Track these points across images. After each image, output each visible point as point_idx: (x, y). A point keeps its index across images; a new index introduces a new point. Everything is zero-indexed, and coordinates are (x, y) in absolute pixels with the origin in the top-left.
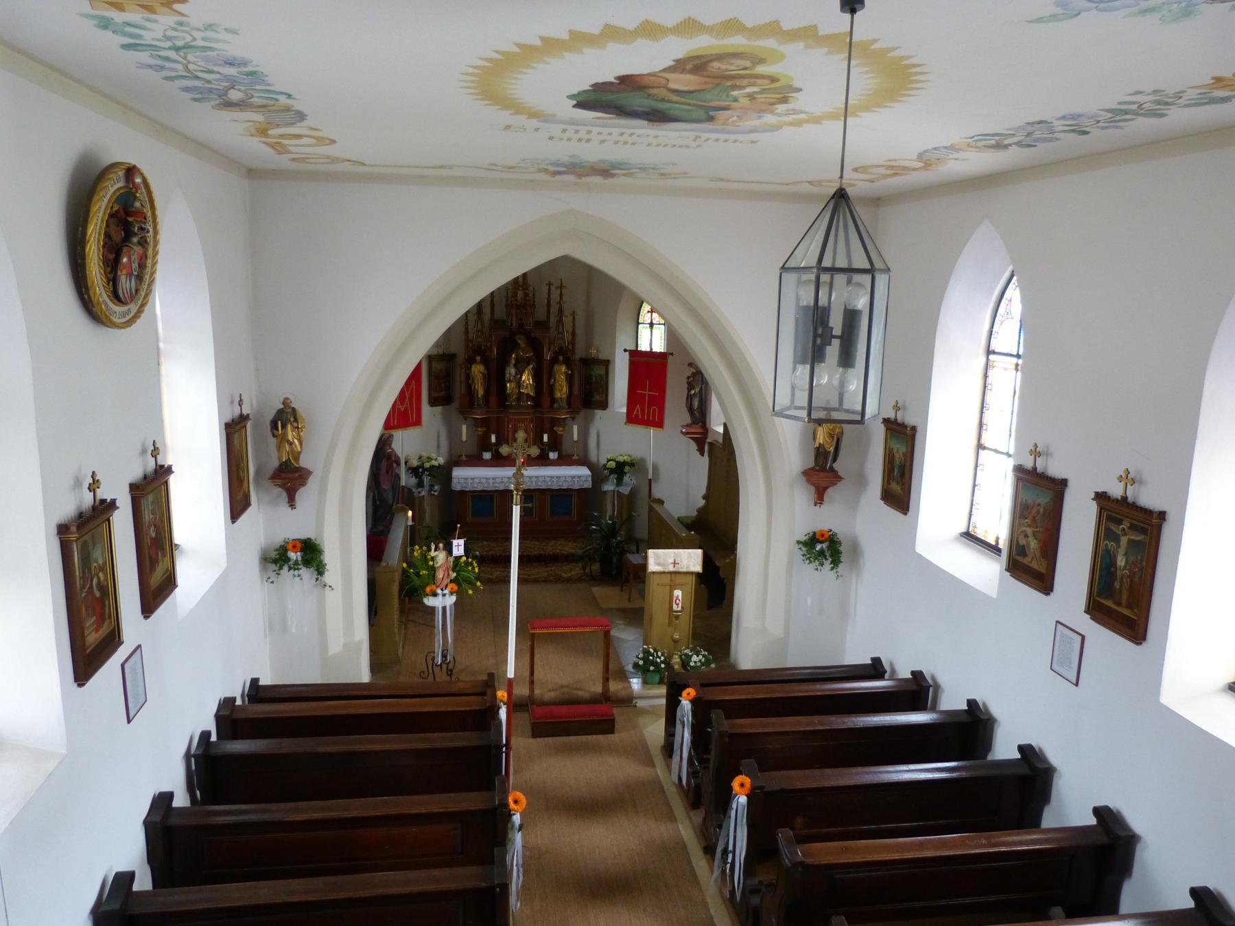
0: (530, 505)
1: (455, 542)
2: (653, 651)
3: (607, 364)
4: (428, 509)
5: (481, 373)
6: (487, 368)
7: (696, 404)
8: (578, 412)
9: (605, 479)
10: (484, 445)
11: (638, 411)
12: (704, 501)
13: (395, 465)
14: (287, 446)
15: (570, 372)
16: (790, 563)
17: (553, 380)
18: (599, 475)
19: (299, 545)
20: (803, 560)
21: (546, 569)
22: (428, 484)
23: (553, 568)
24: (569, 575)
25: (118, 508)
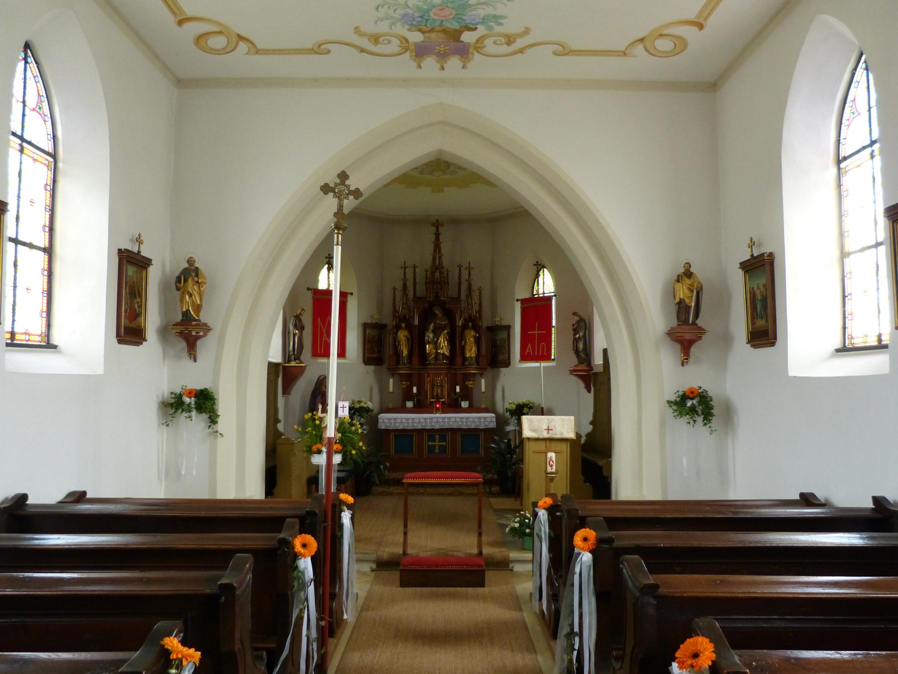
0: (444, 443)
3: (508, 328)
5: (405, 336)
7: (581, 346)
10: (408, 395)
11: (529, 349)
12: (591, 426)
14: (187, 297)
15: (478, 335)
16: (663, 424)
17: (463, 342)
20: (674, 416)
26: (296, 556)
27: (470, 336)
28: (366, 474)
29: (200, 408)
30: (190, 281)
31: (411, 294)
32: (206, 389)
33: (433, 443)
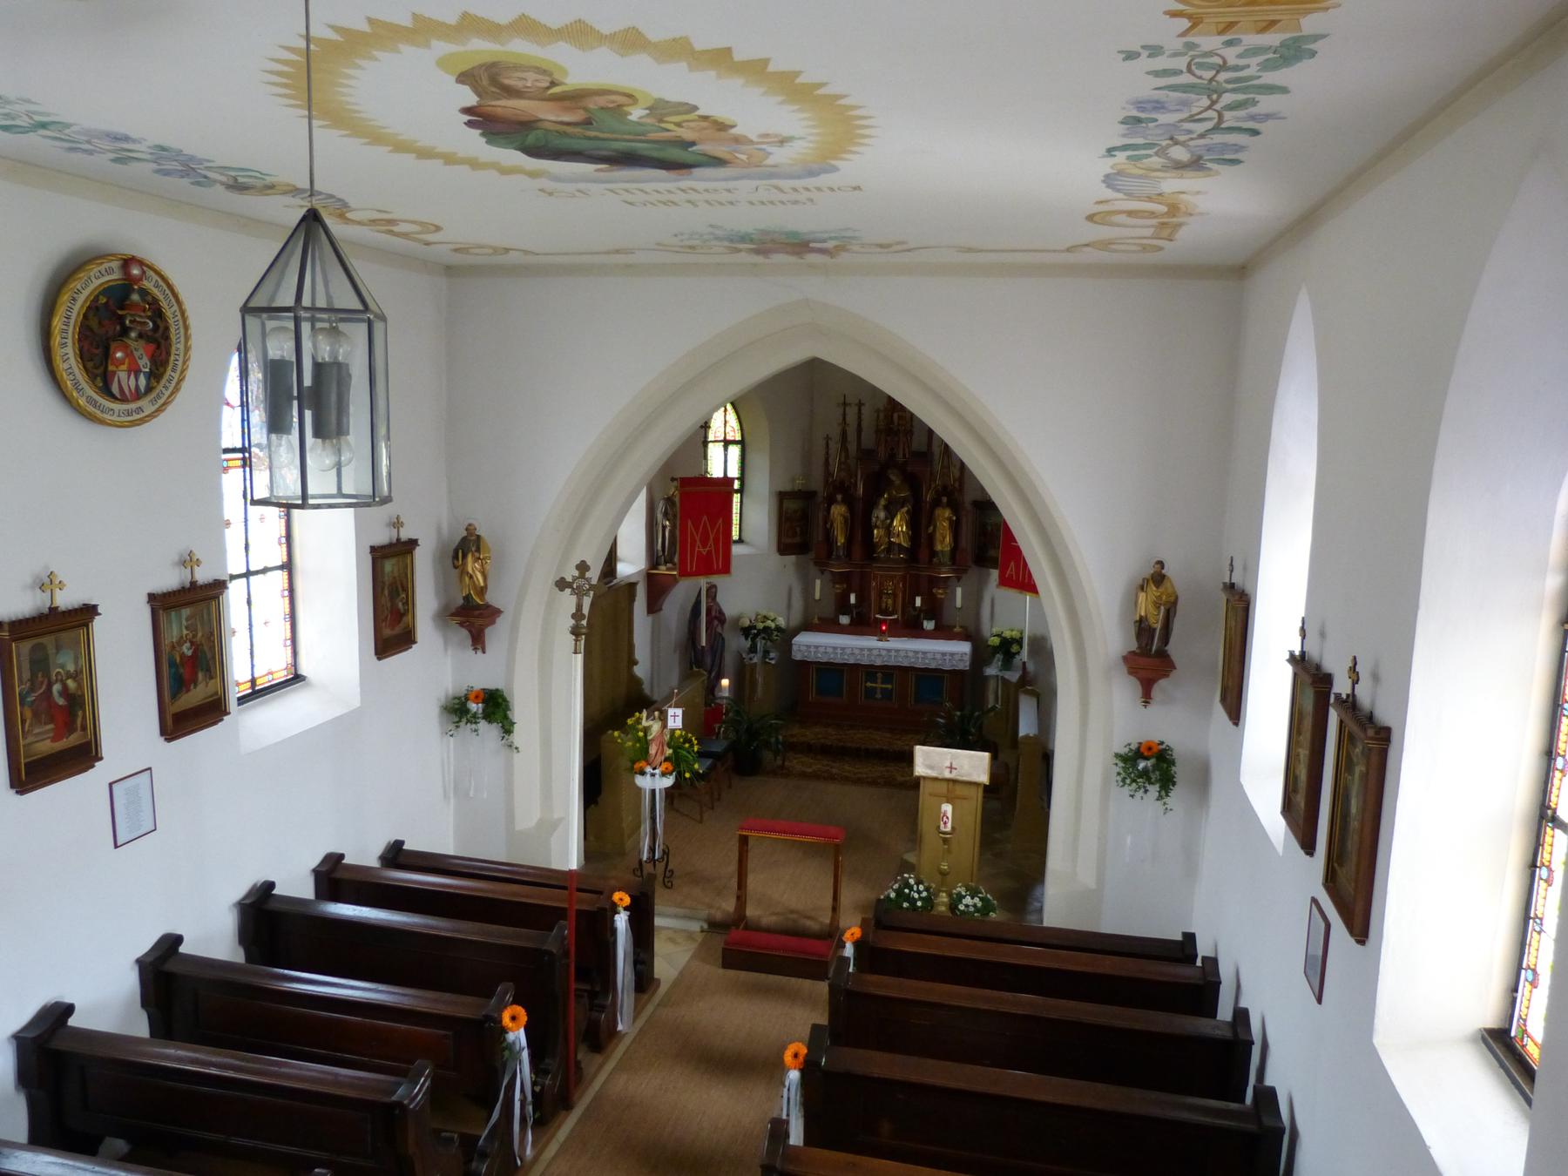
1: (671, 711)
2: (913, 883)
4: (760, 680)
5: (841, 515)
8: (965, 571)
9: (988, 663)
10: (843, 607)
13: (716, 622)
14: (467, 579)
15: (954, 518)
17: (932, 528)
18: (982, 653)
19: (482, 695)
25: (100, 614)
26: (504, 1031)
27: (944, 516)
28: (755, 745)
29: (488, 716)
30: (470, 558)
31: (852, 447)
32: (497, 690)
33: (874, 685)
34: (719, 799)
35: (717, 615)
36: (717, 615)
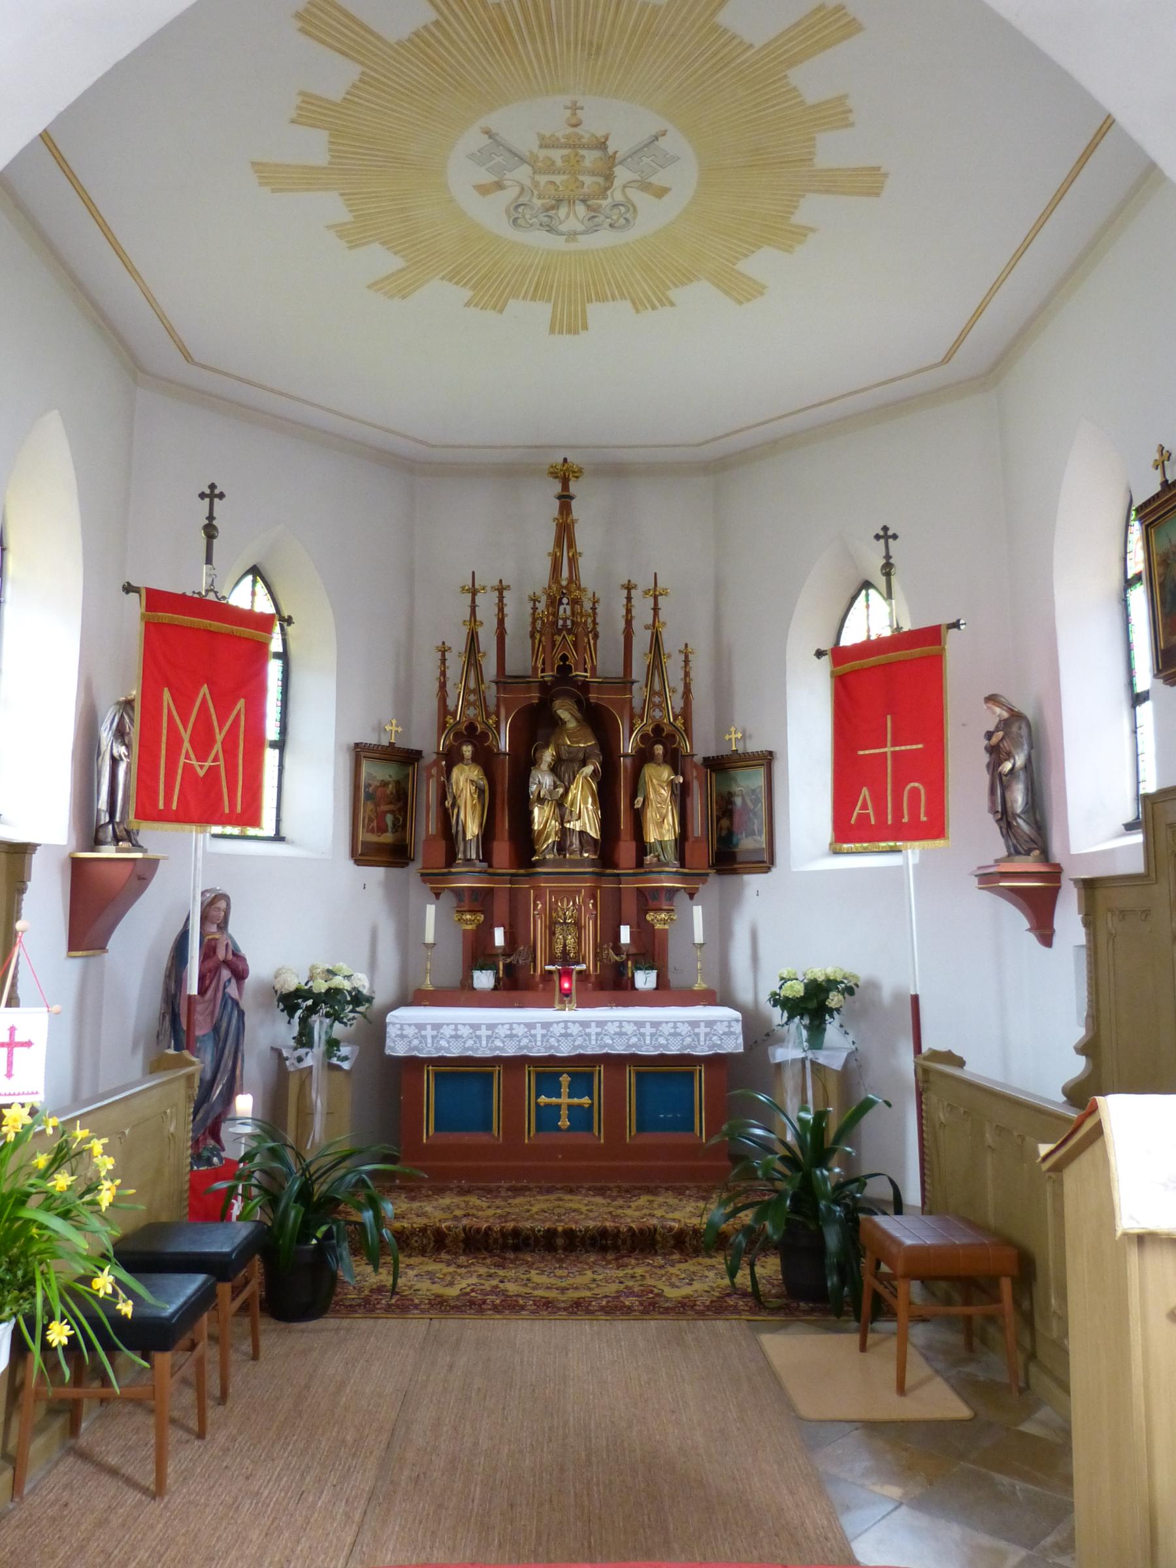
0: (586, 1100)
6: (489, 773)
7: (1018, 797)
11: (864, 807)
13: (226, 974)
21: (621, 1273)
22: (324, 1037)
23: (639, 1271)
24: (686, 1291)
28: (319, 1234)
34: (223, 1398)
35: (230, 957)
36: (230, 957)
